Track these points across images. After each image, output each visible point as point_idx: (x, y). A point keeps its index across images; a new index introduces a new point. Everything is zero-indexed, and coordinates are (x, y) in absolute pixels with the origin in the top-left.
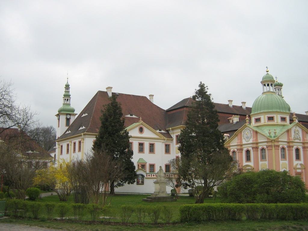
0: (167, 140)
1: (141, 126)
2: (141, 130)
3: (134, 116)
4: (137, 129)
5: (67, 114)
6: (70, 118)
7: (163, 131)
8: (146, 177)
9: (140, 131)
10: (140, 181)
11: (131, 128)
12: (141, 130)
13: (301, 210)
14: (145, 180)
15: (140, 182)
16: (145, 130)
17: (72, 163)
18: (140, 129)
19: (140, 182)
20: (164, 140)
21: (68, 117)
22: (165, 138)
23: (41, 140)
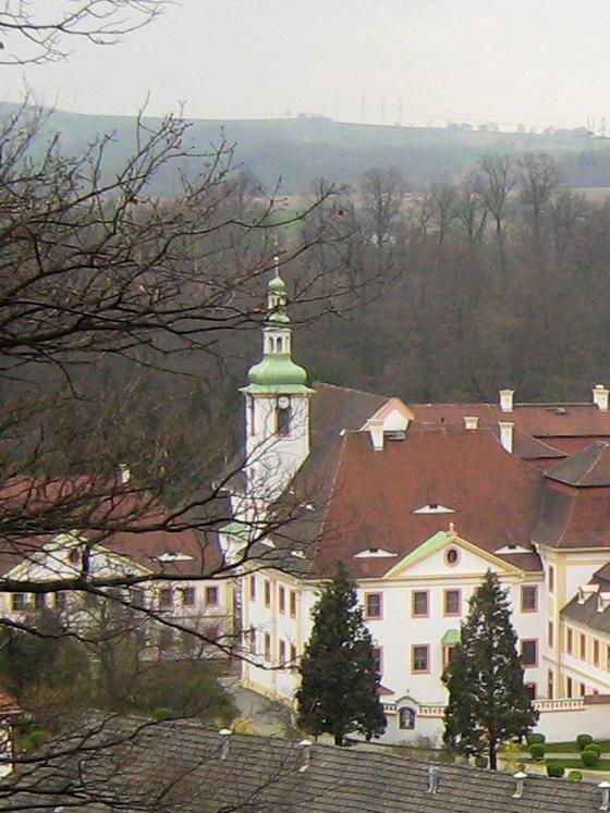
0: (527, 575)
1: (453, 546)
2: (452, 556)
3: (441, 509)
4: (442, 556)
5: (278, 396)
6: (290, 407)
7: (519, 550)
8: (418, 713)
9: (449, 559)
10: (408, 721)
11: (413, 559)
12: (452, 556)
13: (607, 776)
14: (417, 720)
15: (407, 725)
16: (463, 554)
17: (193, 683)
18: (449, 555)
19: (407, 725)
20: (519, 576)
21: (284, 403)
22: (520, 571)
23: (341, 274)
